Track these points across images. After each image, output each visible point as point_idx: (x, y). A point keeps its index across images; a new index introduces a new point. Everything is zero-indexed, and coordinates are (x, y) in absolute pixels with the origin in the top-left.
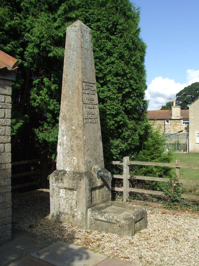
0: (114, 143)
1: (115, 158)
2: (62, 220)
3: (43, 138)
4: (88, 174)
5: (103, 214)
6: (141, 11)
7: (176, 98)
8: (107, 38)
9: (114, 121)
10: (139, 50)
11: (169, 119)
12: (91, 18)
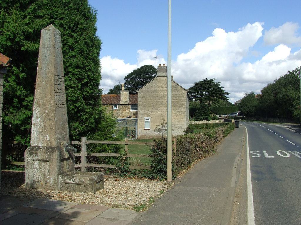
0: (74, 125)
1: (74, 138)
2: (36, 187)
3: (8, 121)
4: (59, 148)
5: (72, 178)
6: (98, 13)
7: (125, 81)
8: (70, 35)
9: (74, 106)
10: (96, 46)
11: (117, 104)
12: (55, 15)
